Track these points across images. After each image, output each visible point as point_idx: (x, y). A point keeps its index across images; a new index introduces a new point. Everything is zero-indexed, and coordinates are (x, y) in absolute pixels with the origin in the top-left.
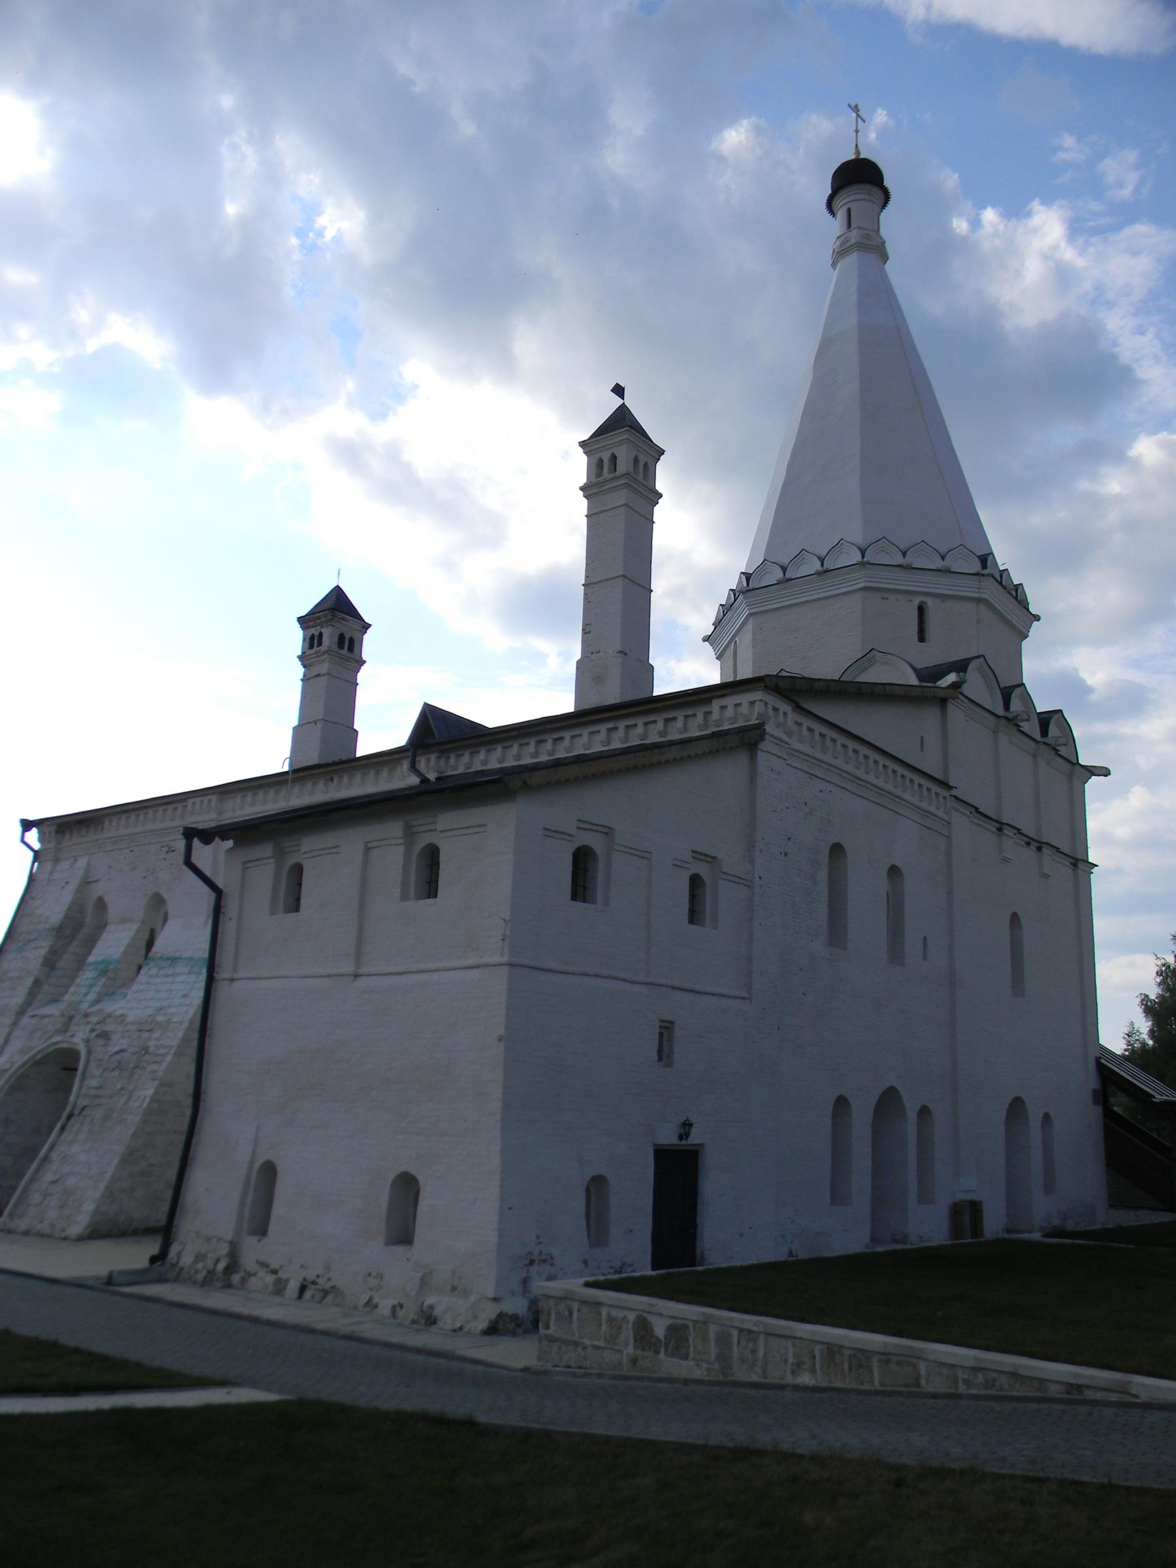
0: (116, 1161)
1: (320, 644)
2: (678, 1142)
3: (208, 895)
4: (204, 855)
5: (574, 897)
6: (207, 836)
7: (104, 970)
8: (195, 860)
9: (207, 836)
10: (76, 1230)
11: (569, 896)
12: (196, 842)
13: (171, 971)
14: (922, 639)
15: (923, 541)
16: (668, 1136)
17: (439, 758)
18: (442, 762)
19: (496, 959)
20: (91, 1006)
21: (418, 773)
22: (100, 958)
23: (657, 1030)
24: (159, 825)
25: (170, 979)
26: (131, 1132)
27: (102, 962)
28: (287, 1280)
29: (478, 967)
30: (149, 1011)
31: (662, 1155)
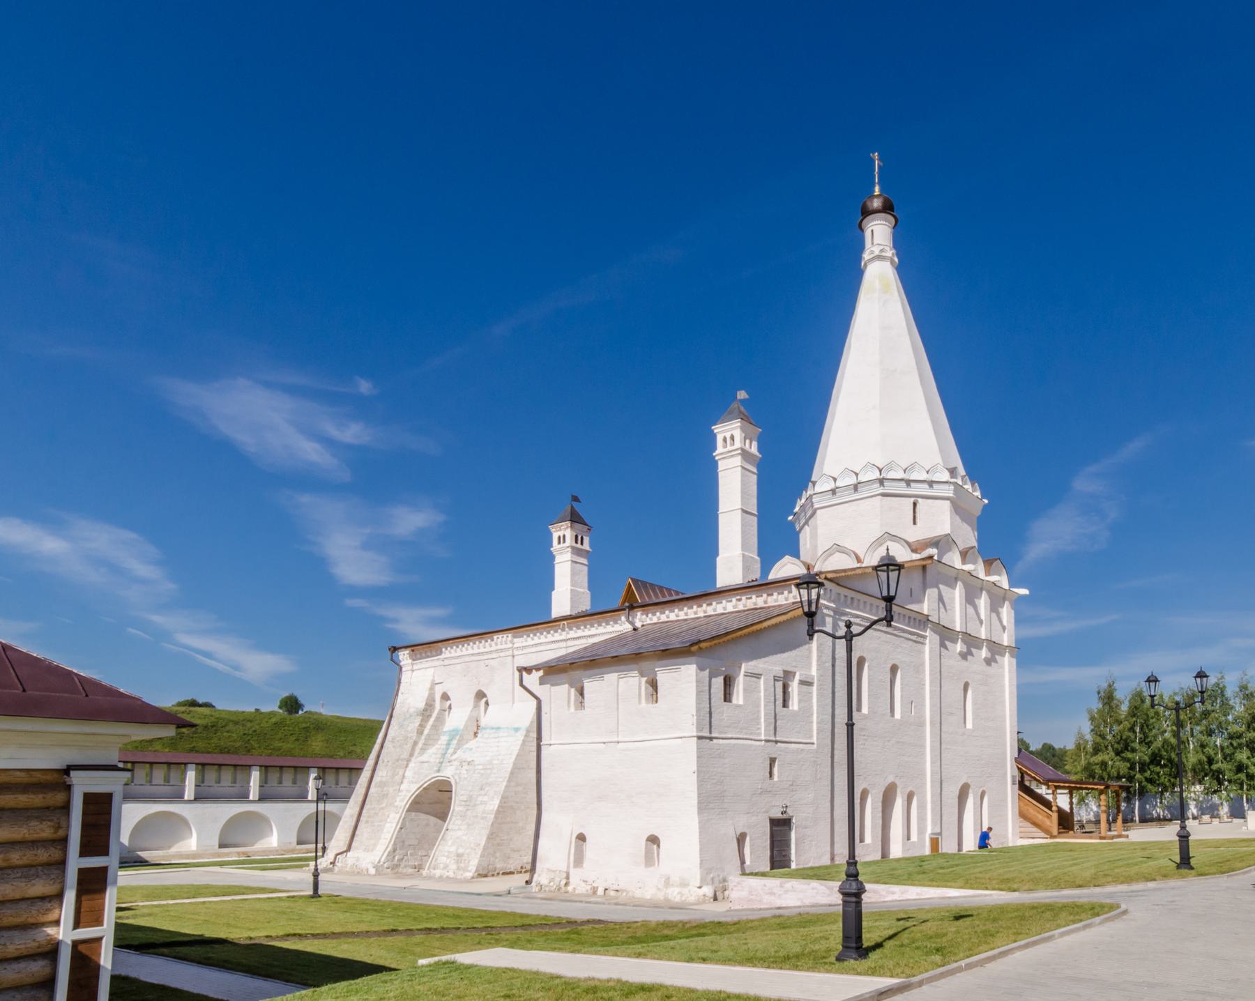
0: (485, 839)
1: (564, 542)
2: (781, 815)
3: (534, 702)
4: (532, 680)
5: (725, 701)
6: (528, 670)
7: (454, 734)
8: (525, 683)
9: (528, 670)
10: (469, 875)
11: (723, 700)
12: (524, 673)
13: (496, 735)
14: (915, 523)
15: (744, 874)
16: (777, 814)
17: (642, 614)
18: (644, 616)
19: (690, 734)
20: (452, 755)
21: (632, 623)
22: (451, 728)
23: (769, 762)
24: (476, 651)
25: (497, 740)
26: (490, 823)
27: (453, 731)
28: (597, 888)
29: (681, 738)
30: (488, 758)
31: (774, 823)
